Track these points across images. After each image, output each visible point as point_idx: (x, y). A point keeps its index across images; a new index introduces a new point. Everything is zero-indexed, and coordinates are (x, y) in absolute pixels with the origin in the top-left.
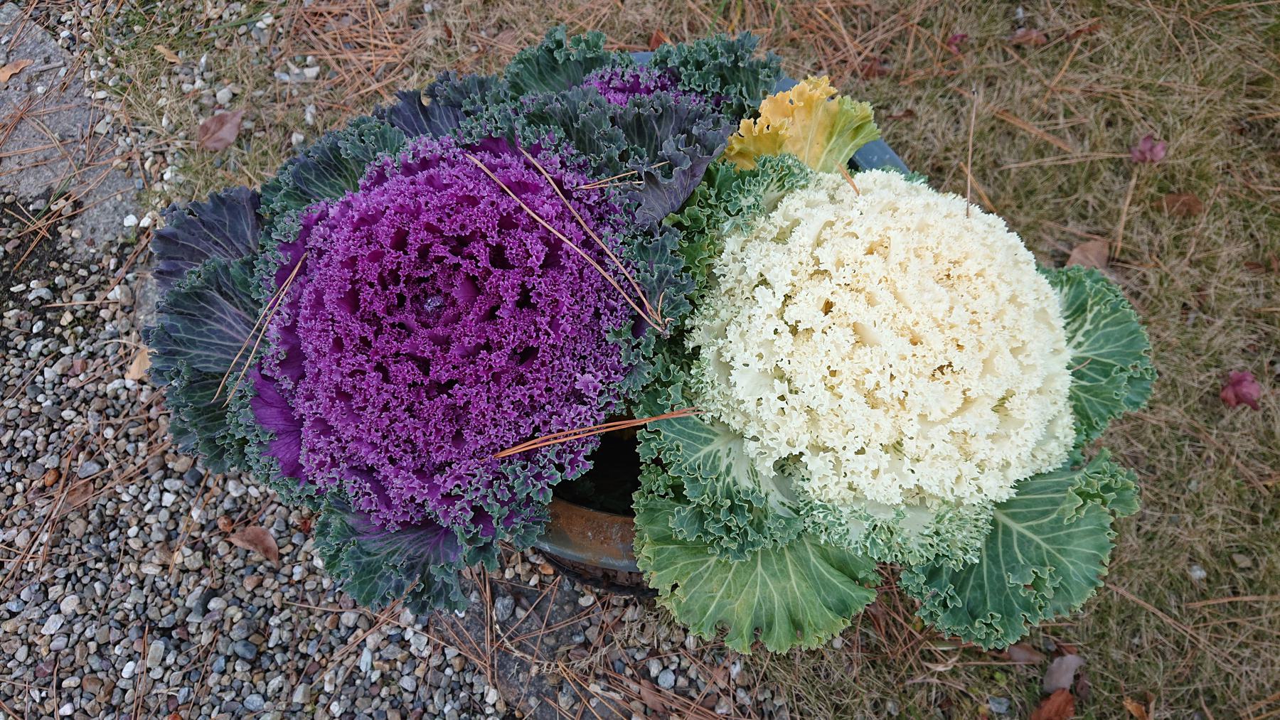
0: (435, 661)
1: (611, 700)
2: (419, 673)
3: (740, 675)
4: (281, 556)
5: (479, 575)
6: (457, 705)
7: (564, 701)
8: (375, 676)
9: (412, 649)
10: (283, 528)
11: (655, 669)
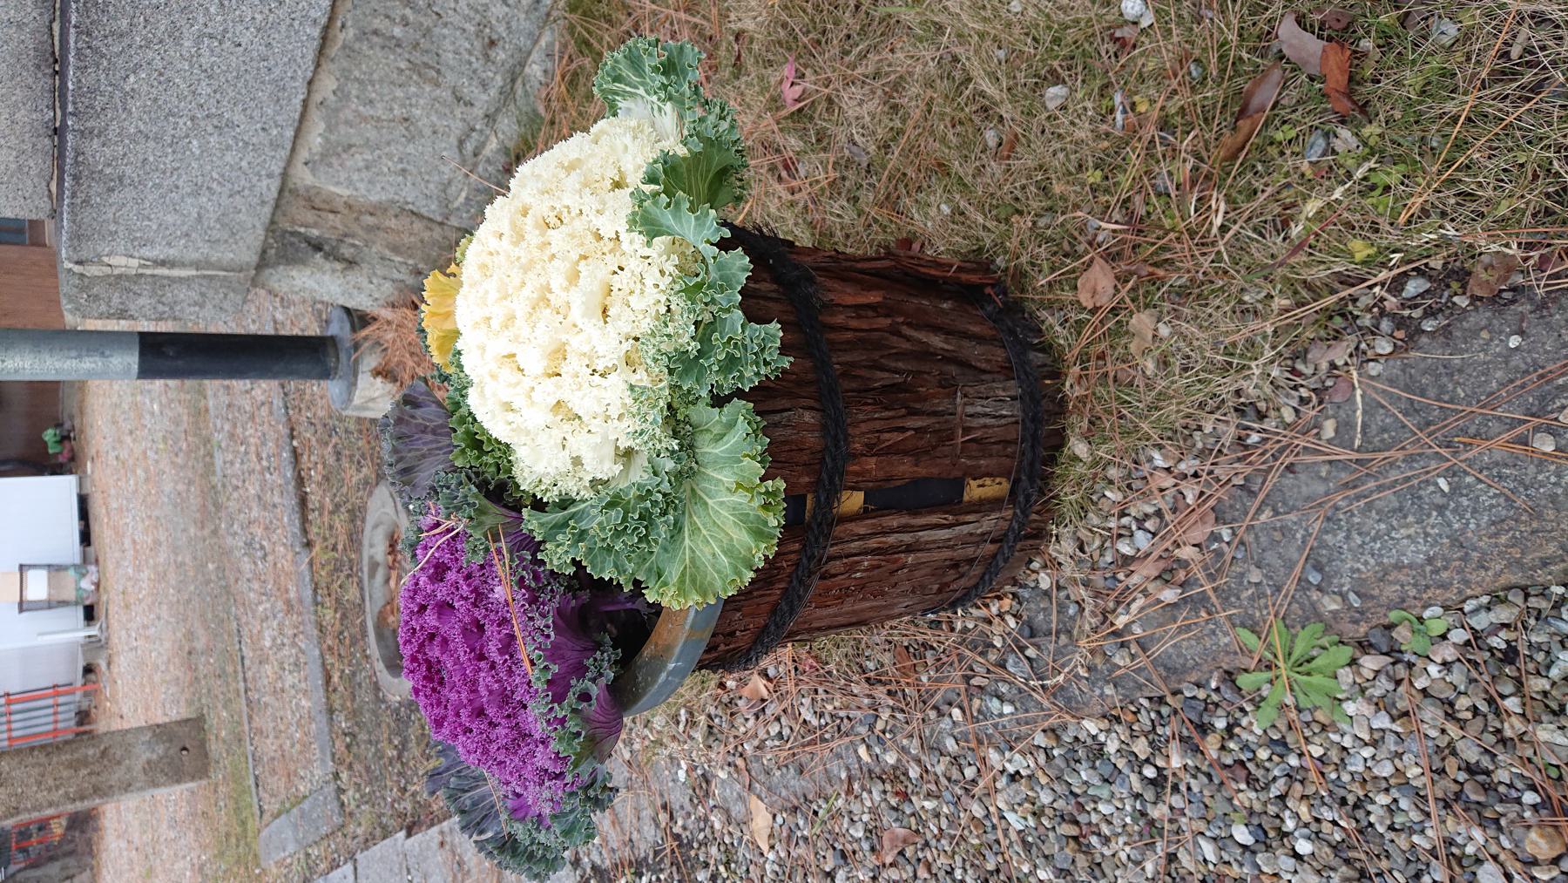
0: (1042, 759)
1: (1142, 609)
2: (1044, 780)
3: (1165, 457)
4: (917, 831)
5: (989, 671)
6: (1085, 764)
7: (1120, 659)
8: (1031, 822)
9: (1023, 773)
10: (895, 815)
11: (1125, 548)
